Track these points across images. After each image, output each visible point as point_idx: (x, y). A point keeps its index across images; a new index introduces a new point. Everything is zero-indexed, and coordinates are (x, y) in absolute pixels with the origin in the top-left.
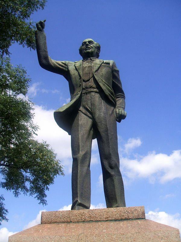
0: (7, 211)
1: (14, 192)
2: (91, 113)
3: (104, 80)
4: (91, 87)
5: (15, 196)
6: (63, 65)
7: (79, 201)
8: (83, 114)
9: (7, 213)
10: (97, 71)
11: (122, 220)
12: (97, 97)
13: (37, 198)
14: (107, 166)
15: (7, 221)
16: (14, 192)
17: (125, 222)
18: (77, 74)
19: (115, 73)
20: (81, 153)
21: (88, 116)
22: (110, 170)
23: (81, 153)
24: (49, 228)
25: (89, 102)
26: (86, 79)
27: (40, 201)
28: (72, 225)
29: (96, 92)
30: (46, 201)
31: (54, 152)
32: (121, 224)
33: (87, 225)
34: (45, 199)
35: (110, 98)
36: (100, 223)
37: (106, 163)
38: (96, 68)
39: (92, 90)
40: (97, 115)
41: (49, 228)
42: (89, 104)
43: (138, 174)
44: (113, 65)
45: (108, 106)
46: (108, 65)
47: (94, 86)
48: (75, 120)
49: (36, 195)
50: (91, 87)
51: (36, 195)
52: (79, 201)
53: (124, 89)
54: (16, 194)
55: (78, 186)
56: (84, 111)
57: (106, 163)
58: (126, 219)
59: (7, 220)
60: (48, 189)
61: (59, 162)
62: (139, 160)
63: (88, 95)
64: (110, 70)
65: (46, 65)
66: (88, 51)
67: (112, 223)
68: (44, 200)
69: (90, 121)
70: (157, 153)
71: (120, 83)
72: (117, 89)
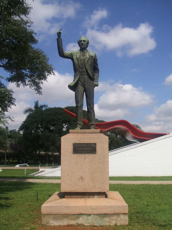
0: (14, 99)
1: (16, 84)
2: (84, 85)
3: (90, 68)
4: (84, 72)
5: (17, 87)
6: (70, 55)
7: (79, 123)
8: (80, 85)
9: (15, 101)
10: (87, 62)
11: (93, 133)
12: (86, 77)
13: (34, 90)
14: (89, 108)
15: (15, 106)
16: (16, 84)
17: (94, 134)
18: (77, 63)
19: (96, 61)
20: (80, 104)
21: (82, 86)
22: (90, 110)
23: (80, 104)
24: (73, 135)
25: (83, 79)
26: (82, 67)
27: (37, 92)
28: (79, 134)
29: (86, 75)
30: (42, 92)
31: (47, 56)
32: (93, 134)
33: (83, 134)
34: (41, 90)
35: (92, 77)
36: (87, 134)
37: (89, 107)
38: (86, 61)
39: (85, 73)
40: (86, 86)
41: (73, 135)
42: (83, 81)
43: (105, 47)
44: (95, 57)
45: (91, 81)
46: (92, 58)
47: (86, 71)
48: (77, 89)
49: (34, 88)
50: (84, 72)
51: (34, 88)
52: (79, 123)
53: (99, 68)
54: (18, 86)
55: (79, 117)
56: (81, 84)
57: (89, 107)
58: (94, 133)
59: (15, 105)
60: (43, 83)
61: (52, 66)
62: (107, 31)
63: (83, 76)
64: (93, 60)
65: (62, 54)
66: (83, 47)
67: (90, 134)
68: (40, 91)
69: (83, 88)
70: (124, 27)
71: (98, 65)
72: (95, 69)
